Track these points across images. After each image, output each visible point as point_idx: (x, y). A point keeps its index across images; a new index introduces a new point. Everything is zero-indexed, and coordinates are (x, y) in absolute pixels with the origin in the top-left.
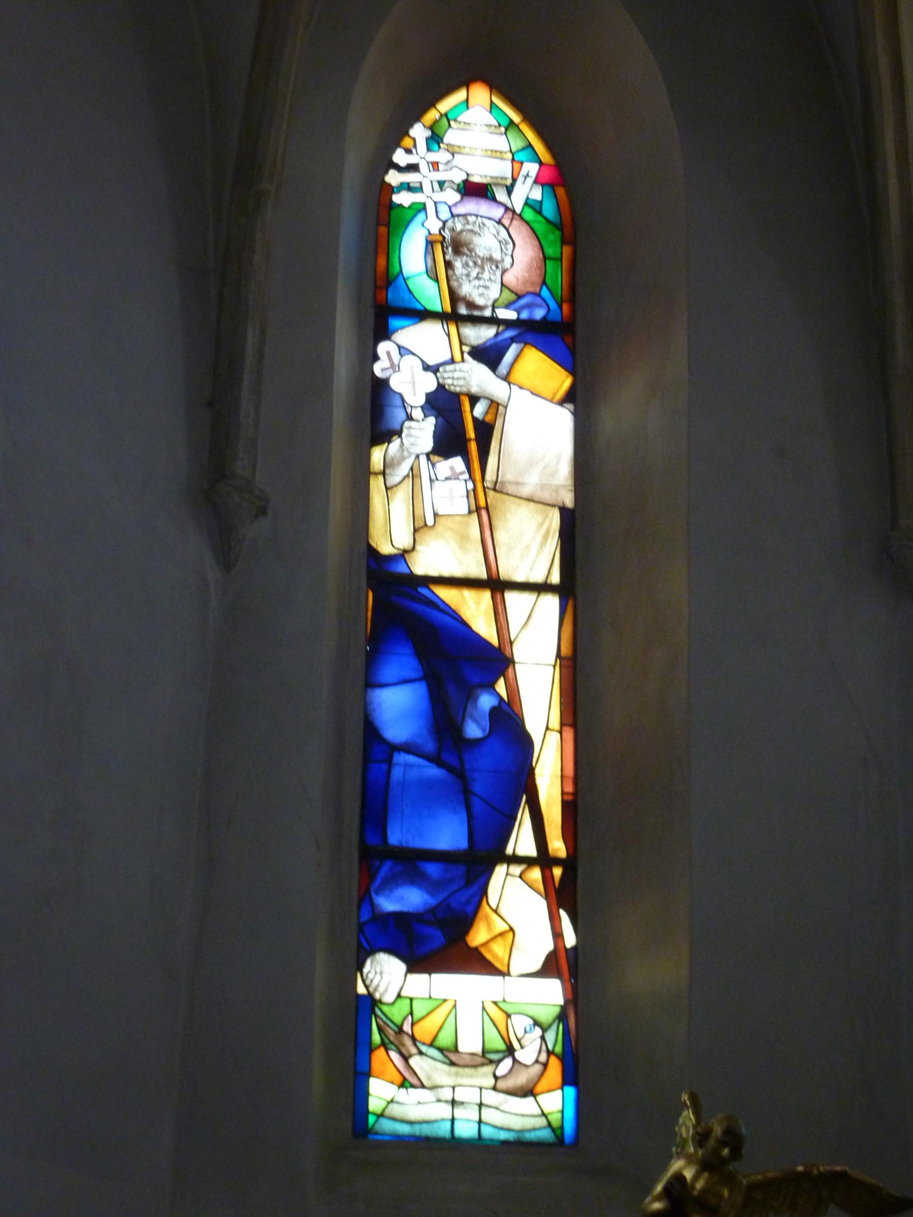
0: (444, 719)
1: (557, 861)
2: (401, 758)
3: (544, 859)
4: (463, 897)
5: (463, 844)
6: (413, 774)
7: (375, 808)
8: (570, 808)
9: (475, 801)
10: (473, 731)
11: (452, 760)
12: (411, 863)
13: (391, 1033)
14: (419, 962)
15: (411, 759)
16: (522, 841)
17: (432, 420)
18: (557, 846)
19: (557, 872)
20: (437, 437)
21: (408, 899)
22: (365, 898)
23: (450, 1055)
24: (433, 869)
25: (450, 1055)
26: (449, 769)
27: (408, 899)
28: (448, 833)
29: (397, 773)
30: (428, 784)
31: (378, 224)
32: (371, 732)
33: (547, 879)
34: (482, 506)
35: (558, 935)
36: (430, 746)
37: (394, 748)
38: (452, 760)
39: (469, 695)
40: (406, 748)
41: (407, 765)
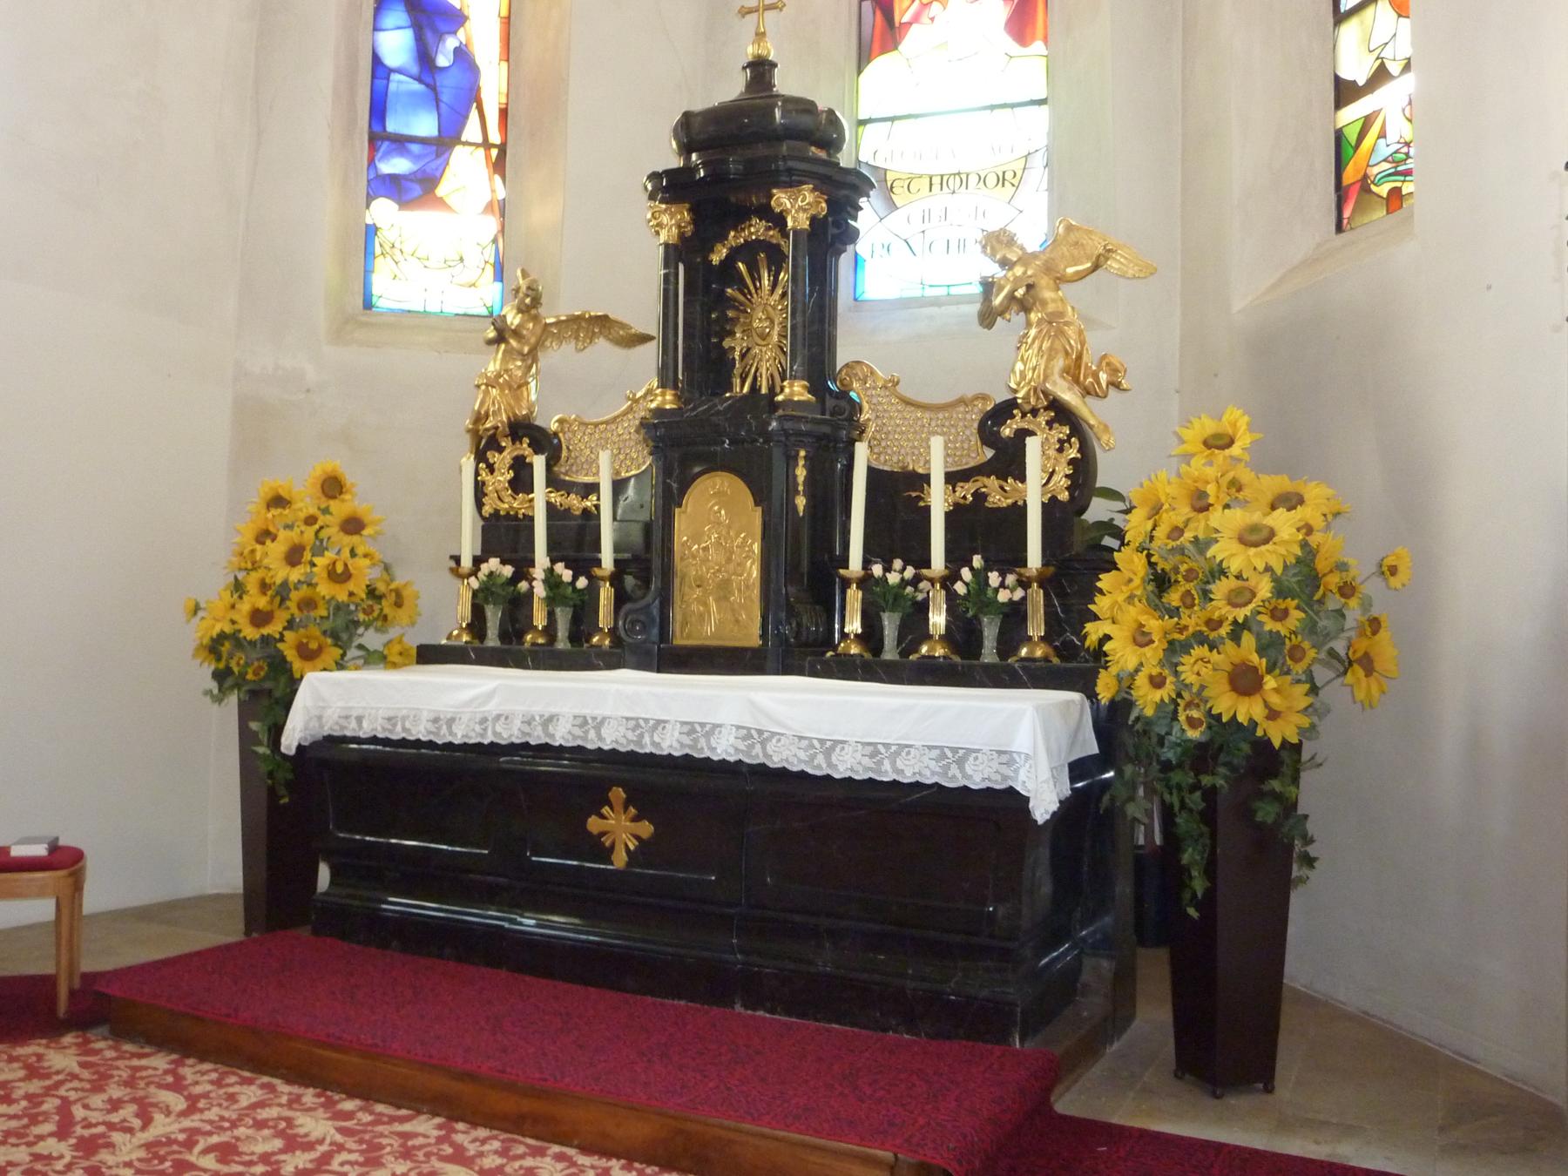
0: (424, 57)
1: (495, 146)
2: (395, 77)
3: (486, 144)
4: (433, 165)
5: (435, 133)
6: (403, 87)
7: (378, 110)
8: (504, 113)
9: (443, 106)
10: (443, 61)
11: (428, 80)
12: (401, 143)
13: (387, 248)
14: (404, 202)
15: (402, 77)
16: (472, 131)
17: (759, 509)
18: (495, 137)
19: (494, 152)
20: (1108, 571)
21: (397, 165)
22: (371, 162)
23: (424, 262)
24: (415, 148)
25: (424, 262)
26: (427, 85)
27: (397, 165)
28: (425, 125)
29: (392, 87)
30: (413, 94)
31: (502, 149)
32: (376, 60)
33: (488, 157)
34: (801, 473)
35: (493, 191)
36: (415, 70)
37: (391, 70)
38: (428, 80)
39: (440, 36)
40: (399, 71)
41: (399, 82)
